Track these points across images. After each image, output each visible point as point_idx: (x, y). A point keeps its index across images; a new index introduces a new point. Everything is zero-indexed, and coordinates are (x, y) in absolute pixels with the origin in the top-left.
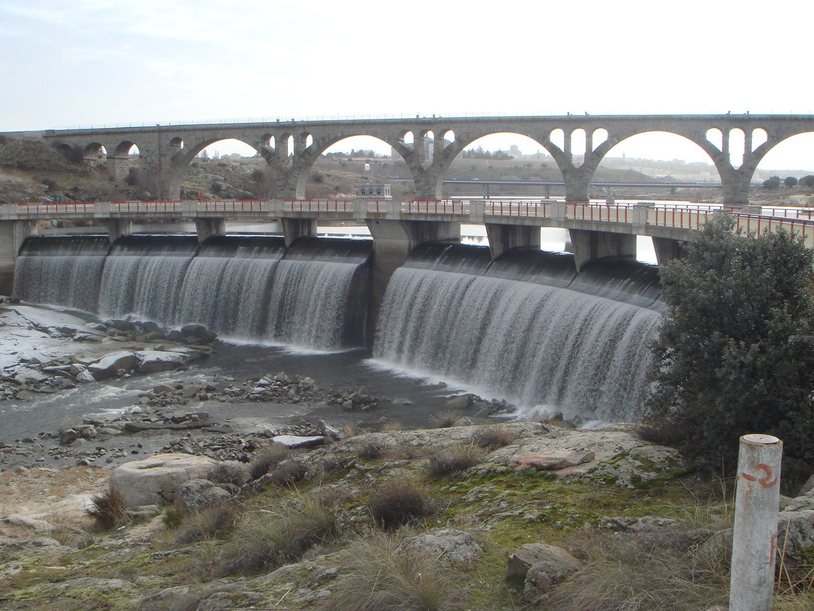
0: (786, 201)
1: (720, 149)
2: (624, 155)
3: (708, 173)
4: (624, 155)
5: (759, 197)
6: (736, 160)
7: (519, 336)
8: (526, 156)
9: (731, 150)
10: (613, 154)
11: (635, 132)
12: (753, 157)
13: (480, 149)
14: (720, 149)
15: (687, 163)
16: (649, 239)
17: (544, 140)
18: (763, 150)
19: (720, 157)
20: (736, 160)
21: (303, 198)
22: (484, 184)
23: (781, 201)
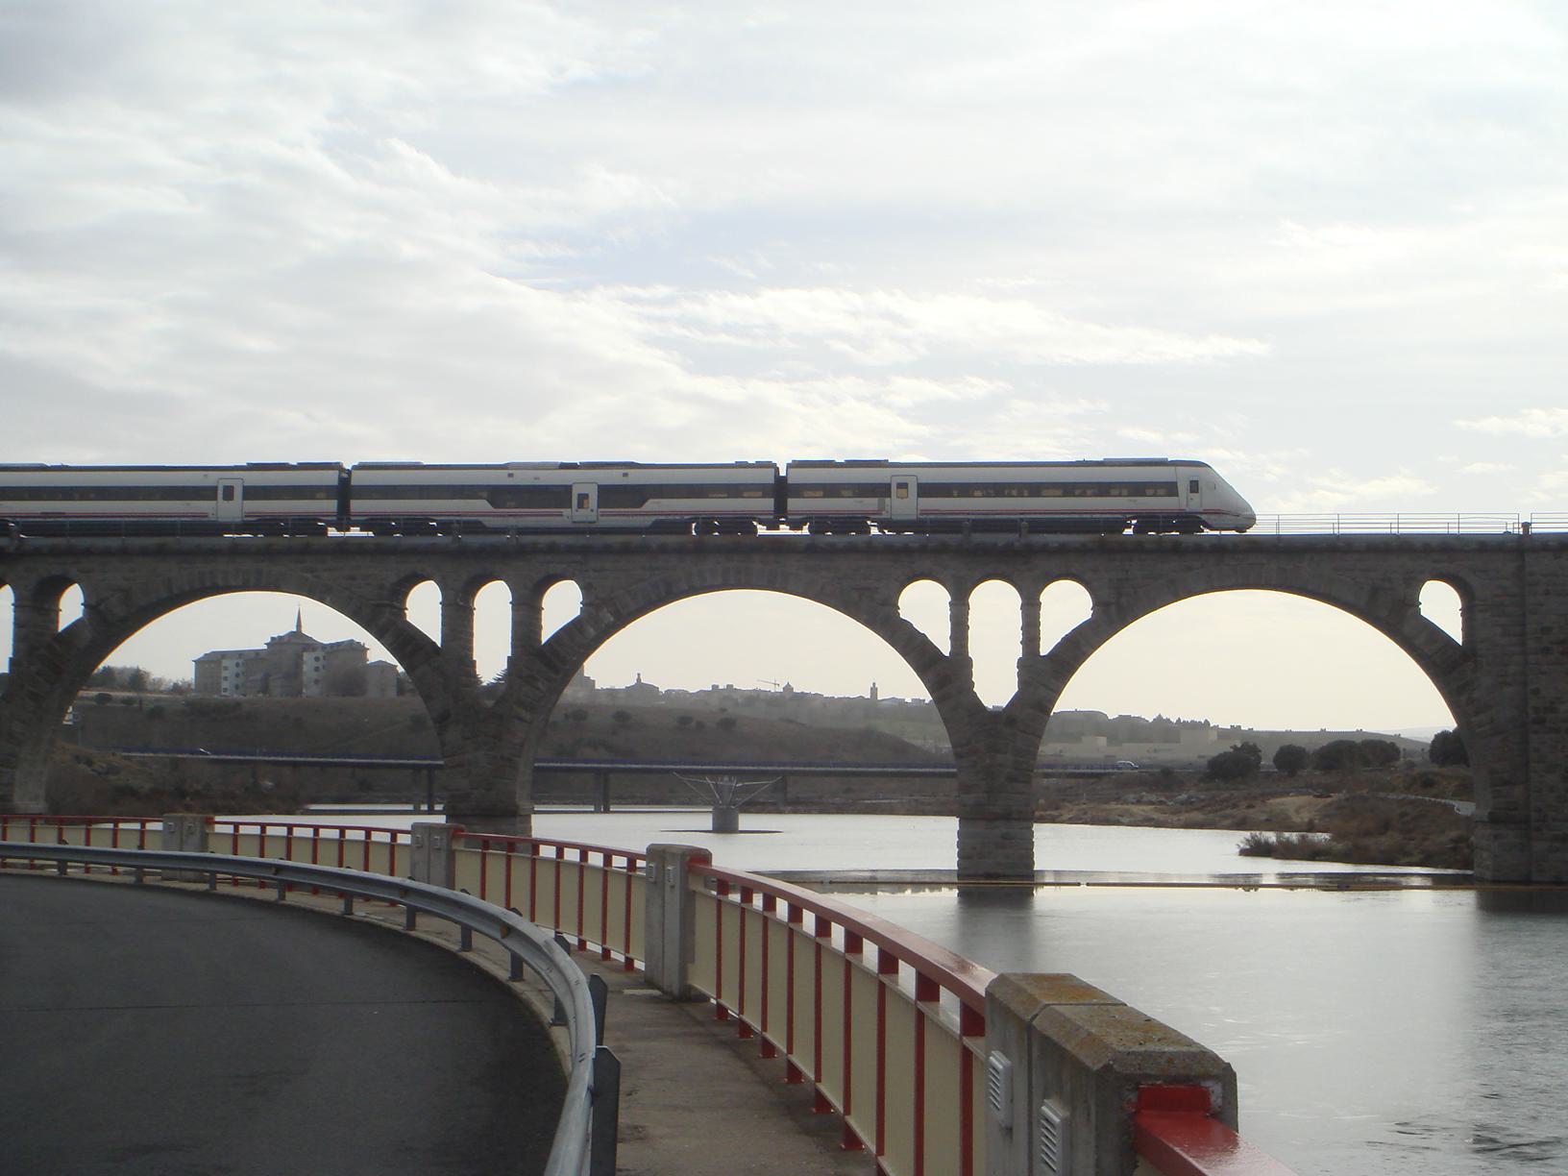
0: (1258, 814)
1: (946, 649)
2: (874, 690)
3: (1102, 741)
4: (874, 690)
5: (1187, 803)
6: (995, 683)
7: (1252, 881)
8: (612, 693)
9: (973, 651)
10: (611, 667)
11: (870, 623)
12: (1046, 671)
13: (788, 688)
14: (946, 649)
15: (662, 689)
16: (876, 948)
17: (382, 614)
18: (1078, 646)
19: (946, 672)
20: (995, 683)
21: (39, 806)
22: (417, 768)
23: (1241, 812)
